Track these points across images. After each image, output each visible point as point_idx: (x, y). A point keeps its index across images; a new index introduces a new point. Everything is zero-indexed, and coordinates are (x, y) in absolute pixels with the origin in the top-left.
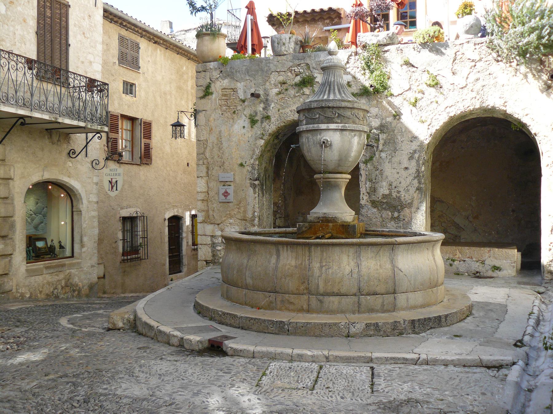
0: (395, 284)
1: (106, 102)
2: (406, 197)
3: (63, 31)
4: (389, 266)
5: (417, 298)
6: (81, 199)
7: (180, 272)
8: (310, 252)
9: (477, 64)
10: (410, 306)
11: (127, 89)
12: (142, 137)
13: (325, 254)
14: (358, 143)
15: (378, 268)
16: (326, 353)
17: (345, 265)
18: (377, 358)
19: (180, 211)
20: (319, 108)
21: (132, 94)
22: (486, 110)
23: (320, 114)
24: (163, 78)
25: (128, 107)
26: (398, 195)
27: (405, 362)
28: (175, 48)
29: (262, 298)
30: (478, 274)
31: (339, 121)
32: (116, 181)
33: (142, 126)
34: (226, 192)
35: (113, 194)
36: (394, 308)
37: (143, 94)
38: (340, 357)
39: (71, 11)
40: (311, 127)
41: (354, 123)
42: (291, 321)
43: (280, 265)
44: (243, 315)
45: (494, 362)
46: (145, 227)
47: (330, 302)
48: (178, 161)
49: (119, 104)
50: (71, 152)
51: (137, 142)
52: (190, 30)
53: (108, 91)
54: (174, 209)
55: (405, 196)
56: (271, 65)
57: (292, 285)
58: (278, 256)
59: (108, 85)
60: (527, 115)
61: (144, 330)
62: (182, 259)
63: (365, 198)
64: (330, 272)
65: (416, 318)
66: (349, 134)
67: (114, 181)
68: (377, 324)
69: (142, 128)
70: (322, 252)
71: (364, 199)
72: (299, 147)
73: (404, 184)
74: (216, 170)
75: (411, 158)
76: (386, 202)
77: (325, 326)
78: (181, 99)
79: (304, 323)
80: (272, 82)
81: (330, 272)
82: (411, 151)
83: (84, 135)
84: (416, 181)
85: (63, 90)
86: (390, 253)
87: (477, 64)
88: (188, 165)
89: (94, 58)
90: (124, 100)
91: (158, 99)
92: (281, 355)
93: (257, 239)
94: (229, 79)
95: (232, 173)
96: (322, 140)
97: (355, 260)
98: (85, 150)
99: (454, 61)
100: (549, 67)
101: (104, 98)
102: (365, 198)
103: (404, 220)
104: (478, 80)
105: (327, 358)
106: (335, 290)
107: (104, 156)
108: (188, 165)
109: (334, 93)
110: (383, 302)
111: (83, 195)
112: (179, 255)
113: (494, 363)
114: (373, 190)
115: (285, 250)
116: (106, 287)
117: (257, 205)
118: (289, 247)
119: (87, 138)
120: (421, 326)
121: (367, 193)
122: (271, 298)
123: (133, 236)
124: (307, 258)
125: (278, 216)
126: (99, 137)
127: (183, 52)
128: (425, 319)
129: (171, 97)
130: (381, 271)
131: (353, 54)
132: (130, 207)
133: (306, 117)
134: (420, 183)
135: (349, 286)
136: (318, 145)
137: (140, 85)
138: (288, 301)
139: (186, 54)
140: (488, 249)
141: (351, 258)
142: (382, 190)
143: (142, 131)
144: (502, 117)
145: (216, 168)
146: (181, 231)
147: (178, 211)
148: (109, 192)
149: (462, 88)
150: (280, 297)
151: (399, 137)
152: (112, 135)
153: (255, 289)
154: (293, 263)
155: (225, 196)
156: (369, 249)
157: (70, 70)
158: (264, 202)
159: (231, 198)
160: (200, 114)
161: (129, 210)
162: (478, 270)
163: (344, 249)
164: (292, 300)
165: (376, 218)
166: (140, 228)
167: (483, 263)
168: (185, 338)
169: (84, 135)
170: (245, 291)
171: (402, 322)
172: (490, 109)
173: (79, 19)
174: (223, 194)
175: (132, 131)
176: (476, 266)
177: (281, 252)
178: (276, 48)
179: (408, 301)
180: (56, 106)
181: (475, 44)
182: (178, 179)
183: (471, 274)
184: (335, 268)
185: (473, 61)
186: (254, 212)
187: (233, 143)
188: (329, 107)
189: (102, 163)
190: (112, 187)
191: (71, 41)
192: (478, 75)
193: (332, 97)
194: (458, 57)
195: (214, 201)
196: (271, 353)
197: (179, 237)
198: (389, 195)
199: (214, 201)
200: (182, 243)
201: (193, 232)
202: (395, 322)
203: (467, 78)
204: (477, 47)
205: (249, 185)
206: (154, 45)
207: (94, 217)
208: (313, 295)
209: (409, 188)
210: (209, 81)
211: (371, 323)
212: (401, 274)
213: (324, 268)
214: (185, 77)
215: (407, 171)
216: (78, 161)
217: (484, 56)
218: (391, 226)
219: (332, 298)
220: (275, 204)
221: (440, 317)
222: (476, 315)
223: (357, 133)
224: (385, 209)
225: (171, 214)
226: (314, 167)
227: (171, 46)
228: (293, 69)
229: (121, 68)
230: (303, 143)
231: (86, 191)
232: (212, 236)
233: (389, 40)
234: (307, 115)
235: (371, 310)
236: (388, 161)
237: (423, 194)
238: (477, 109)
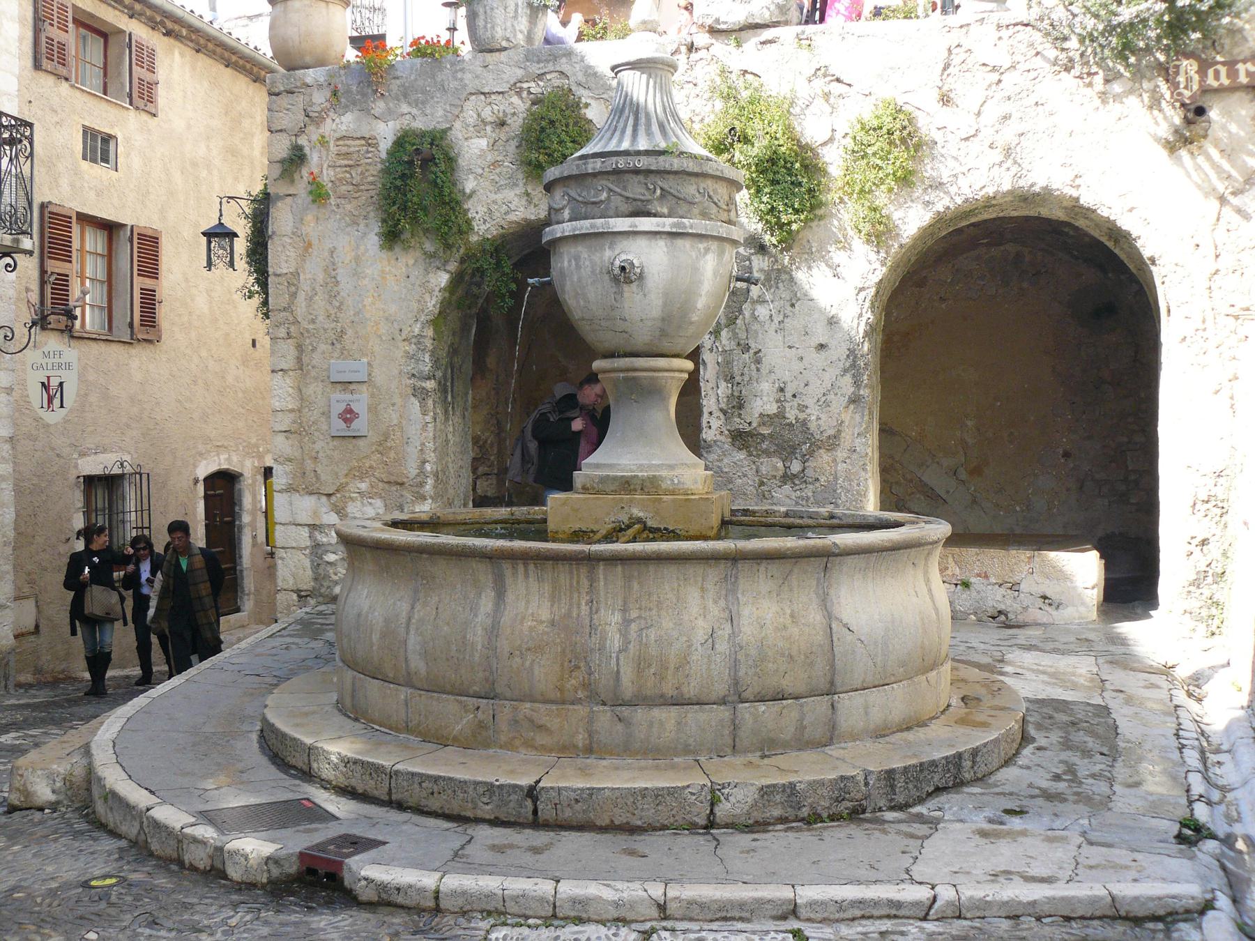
0: (833, 666)
2: (821, 422)
4: (815, 616)
5: (891, 703)
7: (238, 610)
8: (592, 580)
9: (1003, 78)
10: (872, 726)
11: (94, 150)
12: (135, 272)
13: (636, 586)
14: (715, 273)
15: (788, 621)
16: (656, 891)
17: (700, 623)
18: (812, 904)
19: (235, 458)
20: (607, 173)
21: (107, 161)
22: (1026, 198)
23: (611, 190)
24: (189, 127)
25: (98, 195)
26: (802, 416)
27: (893, 912)
28: (219, 50)
29: (454, 714)
30: (1003, 618)
31: (665, 211)
32: (61, 384)
33: (135, 245)
34: (349, 411)
35: (54, 417)
36: (830, 736)
37: (136, 162)
38: (702, 906)
40: (584, 226)
41: (705, 215)
43: (506, 619)
44: (399, 767)
45: (1151, 905)
46: (145, 500)
47: (651, 725)
48: (227, 334)
49: (68, 183)
51: (122, 285)
52: (260, 15)
53: (31, 144)
54: (218, 455)
55: (818, 419)
56: (468, 76)
57: (543, 673)
58: (500, 594)
59: (31, 125)
60: (1131, 210)
61: (110, 815)
62: (242, 578)
63: (715, 424)
64: (653, 637)
65: (897, 764)
66: (692, 246)
67: (54, 383)
68: (792, 786)
69: (135, 250)
70: (628, 579)
71: (713, 427)
72: (549, 283)
73: (816, 389)
74: (324, 353)
76: (771, 435)
77: (644, 797)
78: (236, 179)
79: (582, 790)
80: (471, 121)
81: (653, 637)
84: (848, 379)
86: (818, 579)
87: (1003, 78)
88: (254, 344)
90: (86, 177)
91: (178, 178)
92: (522, 901)
93: (439, 545)
94: (357, 113)
95: (365, 360)
96: (617, 263)
97: (722, 603)
99: (944, 69)
100: (1186, 88)
101: (22, 160)
102: (715, 424)
103: (817, 480)
104: (1006, 118)
105: (662, 907)
106: (668, 689)
107: (27, 316)
108: (254, 344)
109: (649, 133)
110: (801, 720)
112: (234, 569)
113: (1152, 908)
114: (737, 404)
116: (44, 658)
117: (431, 445)
118: (531, 567)
120: (911, 786)
121: (721, 410)
122: (480, 715)
123: (114, 523)
124: (585, 599)
125: (481, 470)
126: (8, 265)
127: (241, 62)
128: (921, 764)
129: (210, 173)
130: (795, 631)
131: (683, 49)
132: (105, 451)
133: (572, 199)
134: (857, 384)
135: (707, 670)
136: (607, 277)
137: (127, 140)
138: (531, 721)
139: (248, 66)
140: (1029, 554)
141: (711, 594)
142: (759, 402)
143: (135, 258)
144: (1060, 215)
145: (322, 347)
146: (237, 509)
147: (229, 460)
148: (41, 413)
149: (967, 139)
150: (506, 711)
152: (54, 266)
153: (435, 687)
154: (545, 615)
155: (346, 420)
156: (762, 568)
158: (450, 436)
159: (360, 425)
161: (101, 457)
162: (1002, 607)
163: (691, 570)
164: (544, 720)
165: (745, 476)
166: (131, 504)
167: (1015, 587)
168: (228, 847)
170: (403, 693)
171: (861, 778)
172: (1038, 194)
174: (341, 416)
175: (110, 257)
176: (999, 598)
177: (509, 580)
178: (480, 32)
179: (866, 713)
181: (999, 27)
182: (230, 380)
183: (985, 618)
184: (667, 624)
185: (994, 69)
186: (424, 462)
187: (366, 282)
188: (637, 172)
189: (21, 332)
190: (50, 401)
192: (1008, 107)
193: (643, 145)
194: (956, 60)
195: (316, 434)
196: (490, 896)
197: (232, 524)
199: (316, 434)
200: (240, 539)
201: (267, 514)
202: (842, 778)
203: (979, 114)
204: (1005, 33)
205: (410, 391)
206: (166, 39)
208: (607, 703)
209: (831, 397)
210: (301, 117)
211: (774, 786)
212: (849, 637)
213: (634, 626)
214: (246, 123)
215: (823, 354)
217: (1022, 59)
218: (783, 500)
219: (658, 713)
220: (476, 440)
221: (959, 756)
222: (1042, 742)
223: (714, 245)
224: (767, 453)
226: (590, 338)
227: (210, 46)
229: (78, 93)
230: (562, 273)
232: (313, 527)
233: (777, 12)
234: (573, 193)
235: (768, 747)
236: (775, 325)
237: (866, 412)
238: (1005, 194)
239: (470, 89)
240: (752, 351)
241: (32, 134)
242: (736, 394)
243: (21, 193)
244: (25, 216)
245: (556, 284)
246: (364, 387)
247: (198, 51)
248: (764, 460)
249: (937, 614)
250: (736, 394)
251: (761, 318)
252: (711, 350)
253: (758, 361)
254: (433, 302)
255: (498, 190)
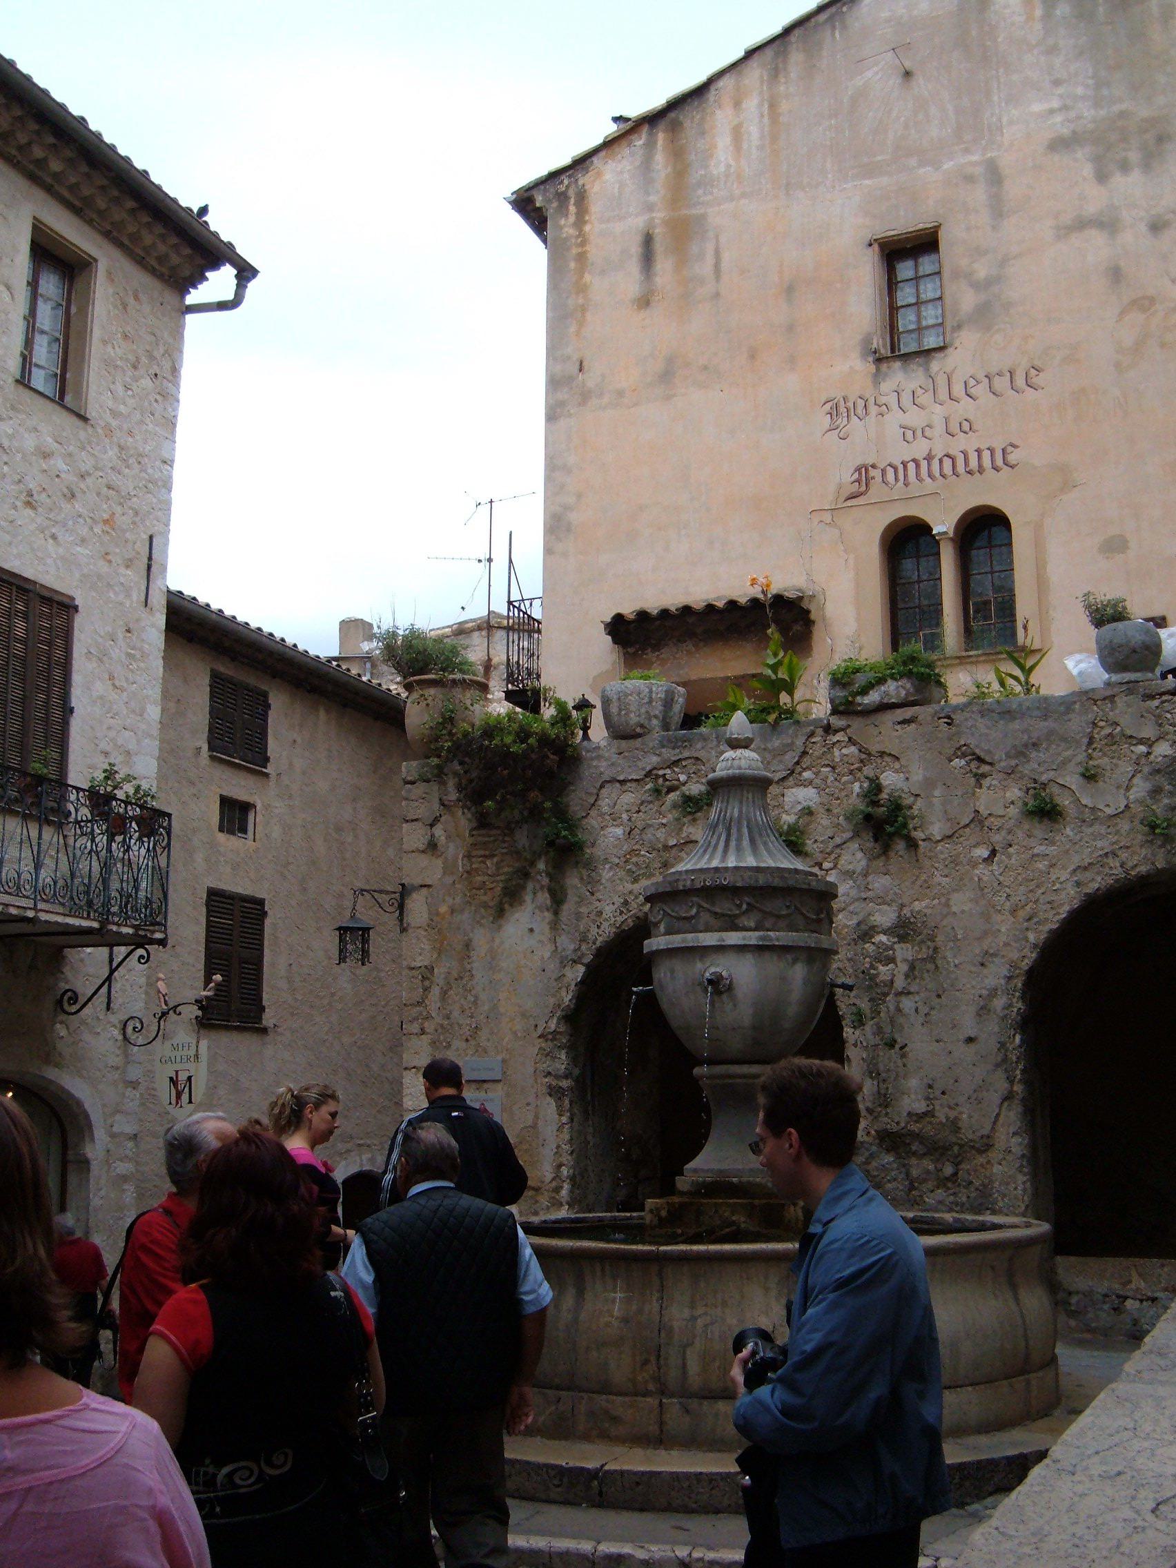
1: (163, 864)
3: (57, 674)
6: (90, 1126)
13: (702, 1285)
23: (700, 906)
26: (952, 1114)
32: (189, 1078)
39: (78, 620)
42: (606, 1468)
43: (583, 1316)
50: (66, 998)
53: (169, 834)
54: (360, 1156)
57: (620, 1367)
58: (580, 1292)
59: (169, 815)
67: (183, 1077)
75: (983, 1011)
77: (699, 1481)
82: (985, 992)
83: (105, 950)
85: (48, 833)
89: (139, 742)
98: (104, 989)
101: (159, 851)
103: (971, 1183)
111: (96, 1117)
115: (599, 1274)
118: (607, 1267)
119: (111, 960)
126: (141, 957)
134: (1011, 1081)
137: (267, 807)
151: (949, 954)
157: (70, 782)
158: (590, 1138)
160: (414, 895)
169: (104, 951)
173: (100, 640)
180: (26, 876)
186: (560, 1166)
191: (78, 698)
198: (925, 1114)
205: (545, 1090)
207: (124, 1178)
210: (436, 806)
216: (83, 1022)
225: (353, 1169)
228: (661, 772)
231: (104, 1106)
239: (606, 777)
240: (897, 1047)
241: (170, 824)
242: (883, 1092)
243: (157, 884)
244: (160, 907)
245: (659, 994)
246: (499, 1086)
247: (345, 706)
248: (914, 1161)
249: (1022, 1316)
250: (883, 1092)
251: (906, 1010)
252: (855, 1045)
253: (903, 1056)
254: (570, 997)
255: (636, 880)
